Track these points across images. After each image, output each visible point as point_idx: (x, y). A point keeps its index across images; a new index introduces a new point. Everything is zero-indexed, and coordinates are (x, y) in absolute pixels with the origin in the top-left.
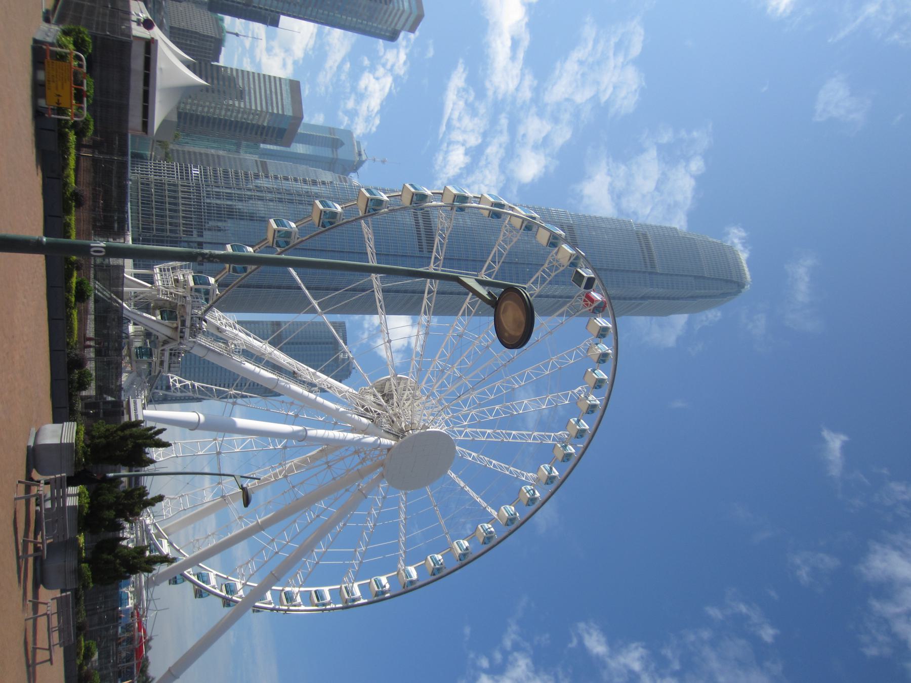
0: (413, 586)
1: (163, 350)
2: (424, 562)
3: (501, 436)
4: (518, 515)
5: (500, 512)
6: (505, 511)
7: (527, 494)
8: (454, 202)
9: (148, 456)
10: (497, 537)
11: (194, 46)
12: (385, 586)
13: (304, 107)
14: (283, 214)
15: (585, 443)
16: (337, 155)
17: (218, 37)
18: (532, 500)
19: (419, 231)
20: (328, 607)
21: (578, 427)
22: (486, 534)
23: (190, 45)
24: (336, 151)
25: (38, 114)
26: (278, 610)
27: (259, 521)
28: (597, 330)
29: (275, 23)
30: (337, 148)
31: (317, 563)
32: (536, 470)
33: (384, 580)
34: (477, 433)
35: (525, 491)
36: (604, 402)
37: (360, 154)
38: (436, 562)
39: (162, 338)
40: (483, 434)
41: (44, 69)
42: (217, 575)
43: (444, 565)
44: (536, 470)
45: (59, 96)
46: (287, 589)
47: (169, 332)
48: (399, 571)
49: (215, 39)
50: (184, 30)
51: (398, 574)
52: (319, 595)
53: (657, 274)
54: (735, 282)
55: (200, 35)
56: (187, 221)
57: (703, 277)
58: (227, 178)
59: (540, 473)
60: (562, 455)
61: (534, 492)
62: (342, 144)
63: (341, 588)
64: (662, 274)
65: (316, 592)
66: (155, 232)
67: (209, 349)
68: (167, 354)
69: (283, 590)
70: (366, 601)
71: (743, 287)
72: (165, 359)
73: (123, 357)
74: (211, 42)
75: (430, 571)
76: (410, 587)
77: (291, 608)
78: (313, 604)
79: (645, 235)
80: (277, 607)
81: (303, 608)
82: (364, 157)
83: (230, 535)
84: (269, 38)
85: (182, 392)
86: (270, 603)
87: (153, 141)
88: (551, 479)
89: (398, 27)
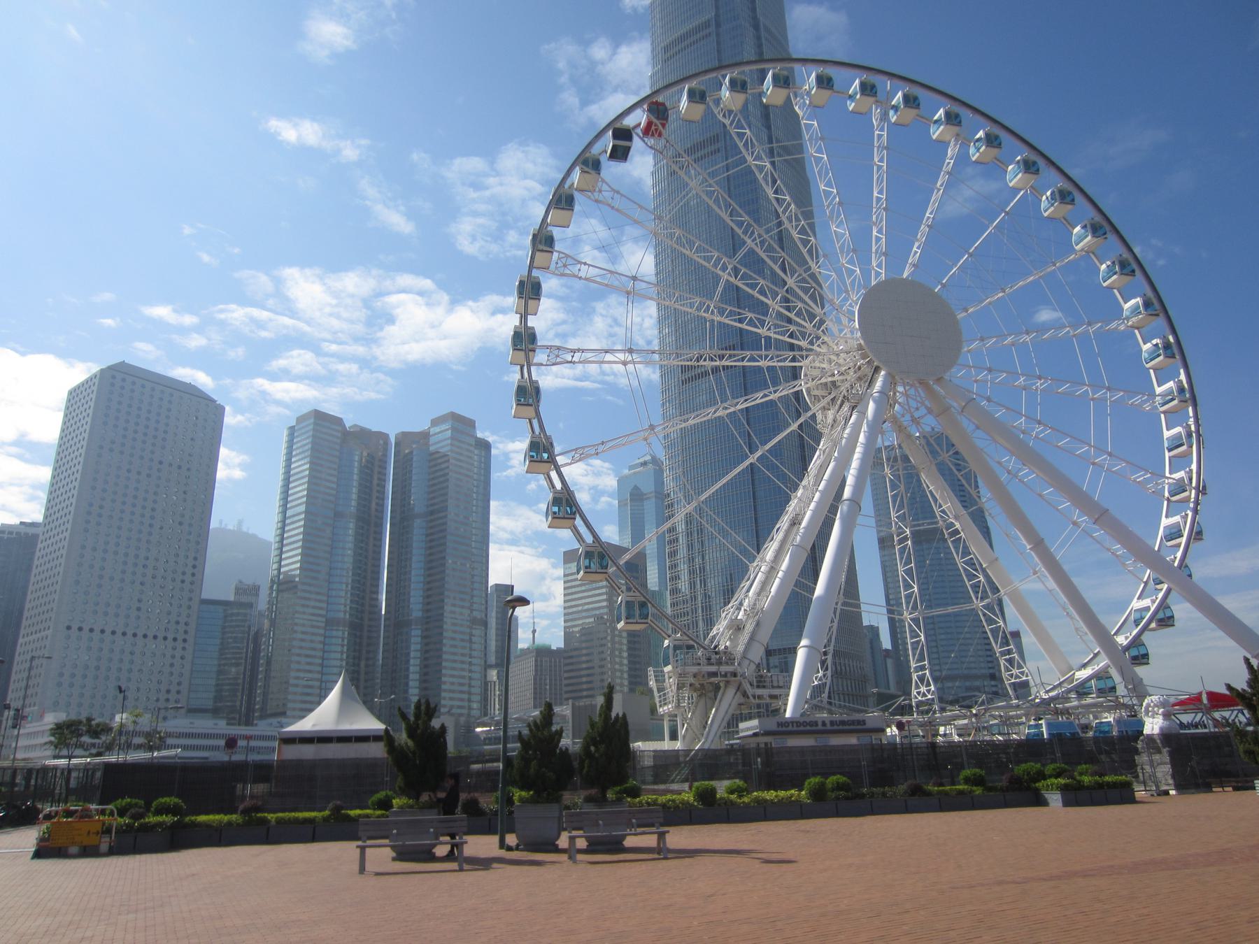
0: (1155, 301)
1: (754, 697)
2: (1115, 291)
3: (879, 214)
4: (1019, 158)
5: (1020, 186)
6: (1015, 180)
7: (981, 150)
8: (522, 350)
9: (538, 721)
10: (1062, 183)
11: (551, 680)
12: (1156, 345)
14: (714, 553)
16: (651, 493)
17: (534, 654)
18: (991, 140)
19: (699, 375)
20: (1193, 428)
21: (858, 96)
22: (1056, 202)
23: (550, 685)
24: (645, 494)
25: (113, 852)
26: (1197, 503)
27: (1028, 547)
30: (643, 494)
31: (1110, 454)
32: (942, 144)
33: (1146, 347)
34: (877, 250)
35: (978, 154)
36: (810, 66)
37: (645, 464)
38: (1110, 271)
39: (739, 697)
40: (878, 239)
41: (67, 848)
42: (1138, 599)
44: (942, 144)
45: (89, 832)
46: (1167, 494)
47: (731, 692)
48: (1131, 327)
49: (537, 657)
50: (535, 693)
51: (1138, 328)
52: (1176, 443)
53: (717, 15)
55: (536, 675)
59: (947, 138)
61: (978, 140)
62: (636, 488)
63: (1164, 412)
64: (717, 8)
65: (1170, 450)
66: (762, 710)
67: (752, 639)
68: (759, 692)
69: (1168, 500)
70: (1182, 371)
74: (541, 661)
75: (1127, 279)
77: (1194, 484)
79: (666, 49)
80: (1192, 505)
81: (1194, 467)
82: (648, 458)
83: (1058, 589)
85: (827, 669)
87: (652, 719)
88: (952, 119)
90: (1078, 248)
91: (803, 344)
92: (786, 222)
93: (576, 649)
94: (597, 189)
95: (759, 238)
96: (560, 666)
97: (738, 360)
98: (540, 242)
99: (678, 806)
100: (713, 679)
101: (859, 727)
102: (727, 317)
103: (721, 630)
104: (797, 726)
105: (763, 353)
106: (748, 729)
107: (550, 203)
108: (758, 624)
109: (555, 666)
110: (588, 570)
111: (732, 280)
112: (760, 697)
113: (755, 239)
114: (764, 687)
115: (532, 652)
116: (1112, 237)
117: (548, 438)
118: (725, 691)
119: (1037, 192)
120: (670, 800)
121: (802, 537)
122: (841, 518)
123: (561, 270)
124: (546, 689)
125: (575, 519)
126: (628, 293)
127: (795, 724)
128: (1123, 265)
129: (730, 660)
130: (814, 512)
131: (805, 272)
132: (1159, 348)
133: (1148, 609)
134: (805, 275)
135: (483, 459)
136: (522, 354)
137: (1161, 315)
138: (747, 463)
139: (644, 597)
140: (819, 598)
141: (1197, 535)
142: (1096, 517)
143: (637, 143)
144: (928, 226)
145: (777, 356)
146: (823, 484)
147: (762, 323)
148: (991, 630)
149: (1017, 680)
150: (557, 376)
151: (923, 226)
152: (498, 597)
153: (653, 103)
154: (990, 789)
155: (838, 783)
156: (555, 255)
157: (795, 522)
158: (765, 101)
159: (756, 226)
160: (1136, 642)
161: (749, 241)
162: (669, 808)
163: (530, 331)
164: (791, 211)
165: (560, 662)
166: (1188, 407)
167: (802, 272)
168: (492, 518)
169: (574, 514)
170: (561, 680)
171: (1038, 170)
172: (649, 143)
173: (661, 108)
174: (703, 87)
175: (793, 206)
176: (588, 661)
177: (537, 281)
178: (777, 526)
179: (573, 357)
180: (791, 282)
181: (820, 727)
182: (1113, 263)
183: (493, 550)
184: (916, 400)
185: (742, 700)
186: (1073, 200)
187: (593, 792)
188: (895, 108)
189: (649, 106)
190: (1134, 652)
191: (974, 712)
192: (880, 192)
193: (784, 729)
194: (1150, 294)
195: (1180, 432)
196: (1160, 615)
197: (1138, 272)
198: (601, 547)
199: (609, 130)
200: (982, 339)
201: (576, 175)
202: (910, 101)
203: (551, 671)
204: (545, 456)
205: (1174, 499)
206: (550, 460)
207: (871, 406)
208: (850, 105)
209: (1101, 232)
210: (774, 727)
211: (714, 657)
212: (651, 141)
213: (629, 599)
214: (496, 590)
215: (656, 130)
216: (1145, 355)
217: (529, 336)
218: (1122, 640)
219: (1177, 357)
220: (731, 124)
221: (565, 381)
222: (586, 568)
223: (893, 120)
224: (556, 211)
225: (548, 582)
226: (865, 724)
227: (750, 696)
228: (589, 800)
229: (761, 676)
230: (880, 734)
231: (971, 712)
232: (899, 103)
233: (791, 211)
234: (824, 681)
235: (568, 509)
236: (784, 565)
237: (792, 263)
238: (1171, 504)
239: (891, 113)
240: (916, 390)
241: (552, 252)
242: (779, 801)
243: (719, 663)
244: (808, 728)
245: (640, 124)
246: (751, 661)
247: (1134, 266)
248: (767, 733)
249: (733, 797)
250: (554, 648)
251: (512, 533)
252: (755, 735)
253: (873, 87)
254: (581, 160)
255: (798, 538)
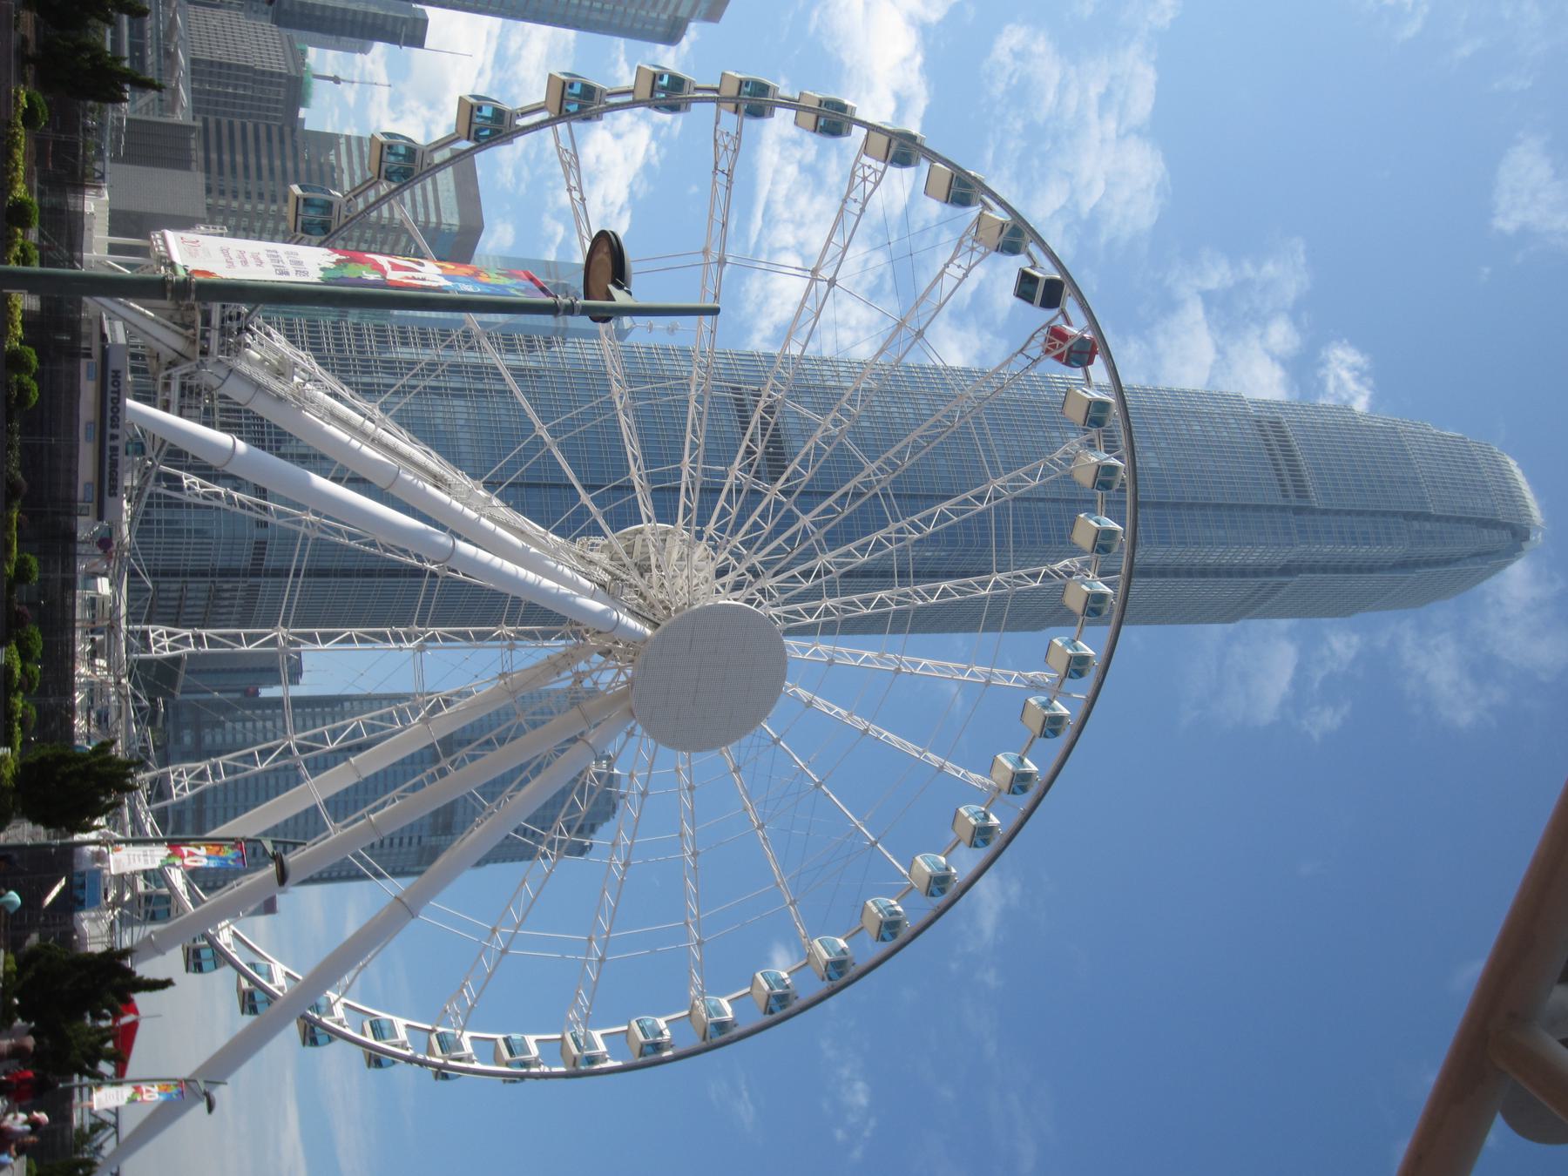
8: (739, 93)
10: (909, 925)
11: (244, 97)
12: (661, 1033)
13: (479, 173)
15: (1089, 691)
20: (534, 1070)
23: (235, 96)
26: (422, 1063)
28: (1084, 409)
29: (414, 34)
31: (504, 952)
32: (990, 767)
39: (167, 355)
42: (287, 974)
43: (792, 989)
44: (990, 767)
46: (440, 1029)
47: (179, 344)
48: (693, 1005)
49: (289, 78)
50: (221, 65)
51: (690, 1015)
53: (1313, 511)
54: (1504, 526)
55: (255, 72)
56: (228, 417)
57: (1427, 517)
58: (315, 326)
60: (1042, 718)
63: (563, 1039)
64: (1325, 512)
65: (506, 1040)
67: (259, 387)
68: (175, 386)
70: (619, 1063)
71: (1527, 538)
72: (172, 400)
73: (98, 1121)
74: (279, 85)
76: (718, 1039)
77: (451, 1063)
78: (497, 1059)
79: (1276, 425)
80: (420, 1056)
81: (477, 1066)
84: (398, 74)
86: (403, 1046)
89: (682, 12)
90: (816, 942)
91: (710, 529)
92: (898, 525)
93: (295, 149)
94: (975, 245)
95: (877, 480)
96: (267, 117)
97: (694, 425)
98: (901, 145)
99: (8, 174)
100: (199, 319)
101: (107, 487)
102: (762, 418)
103: (277, 345)
104: (112, 399)
105: (700, 466)
106: (113, 331)
107: (959, 168)
108: (280, 399)
109: (268, 109)
110: (386, 150)
111: (819, 433)
112: (167, 386)
113: (875, 475)
114: (182, 396)
115: (298, 70)
116: (824, 986)
117: (598, 115)
118: (181, 335)
119: (904, 894)
120: (17, 164)
121: (409, 483)
122: (426, 531)
123: (860, 173)
124: (227, 86)
125: (468, 139)
126: (814, 272)
127: (116, 395)
128: (783, 999)
129: (226, 349)
130: (448, 507)
131: (817, 541)
132: (656, 1036)
133: (271, 980)
134: (813, 540)
135: (650, 27)
136: (734, 92)
137: (704, 1043)
138: (537, 423)
139: (336, 232)
140: (308, 478)
141: (376, 1059)
142: (405, 900)
143: (1043, 316)
144: (867, 730)
145: (693, 483)
146: (490, 525)
147: (746, 469)
148: (252, 754)
149: (172, 783)
150: (777, 172)
151: (867, 723)
152: (405, 21)
153: (1094, 346)
154: (10, 589)
155: (28, 391)
156: (881, 166)
157: (438, 481)
158: (1082, 515)
159: (892, 477)
160: (221, 957)
161: (874, 466)
162: (7, 162)
163: (767, 110)
164: (910, 533)
165: (276, 118)
166: (566, 1066)
167: (817, 536)
168: (545, 30)
169: (476, 140)
170: (242, 116)
171: (932, 895)
172: (1038, 334)
173: (1087, 357)
174: (1108, 424)
175: (917, 536)
176: (272, 170)
177: (845, 131)
178: (433, 453)
179: (723, 172)
180: (806, 520)
181: (110, 431)
182: (787, 987)
183: (489, 24)
184: (613, 681)
185: (164, 360)
186: (883, 939)
187: (32, 49)
188: (1047, 705)
189: (1091, 341)
190: (206, 954)
191: (124, 681)
192: (925, 668)
193: (110, 380)
194: (736, 1031)
195: (530, 1053)
196: (259, 996)
197: (769, 1018)
198: (420, 175)
199: (1061, 274)
200: (691, 788)
201: (999, 215)
202: (1053, 725)
203: (260, 99)
204: (573, 108)
205: (434, 1038)
206: (564, 113)
207: (597, 606)
208: (1061, 641)
209: (833, 974)
210: (114, 364)
211: (235, 325)
212: (1040, 338)
213: (336, 207)
214: (416, 20)
215: (1054, 347)
216: (649, 1020)
217: (760, 107)
218: (225, 938)
219: (640, 1059)
220: (1051, 461)
221: (767, 187)
222: (390, 147)
223: (1032, 701)
224: (948, 177)
225: (424, 111)
226: (110, 495)
227: (169, 372)
228: (24, 41)
229: (199, 394)
230: (96, 515)
231: (124, 676)
232: (1054, 709)
233: (910, 533)
234: (188, 492)
235: (487, 133)
236: (367, 450)
237: (833, 523)
238: (426, 1034)
239: (1043, 699)
240: (623, 683)
241: (885, 161)
242: (9, 308)
243: (224, 332)
244: (109, 414)
245: (1069, 323)
246: (224, 381)
247: (779, 1014)
248: (105, 353)
249: (17, 250)
250: (302, 113)
251: (518, 58)
252: (104, 337)
253: (1080, 674)
254: (1021, 226)
255: (410, 477)
